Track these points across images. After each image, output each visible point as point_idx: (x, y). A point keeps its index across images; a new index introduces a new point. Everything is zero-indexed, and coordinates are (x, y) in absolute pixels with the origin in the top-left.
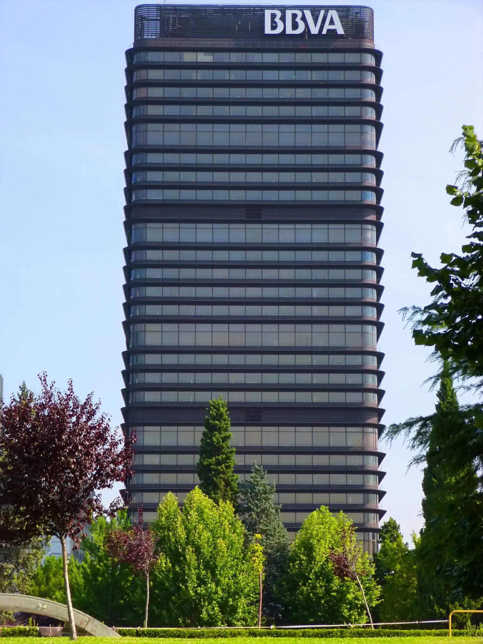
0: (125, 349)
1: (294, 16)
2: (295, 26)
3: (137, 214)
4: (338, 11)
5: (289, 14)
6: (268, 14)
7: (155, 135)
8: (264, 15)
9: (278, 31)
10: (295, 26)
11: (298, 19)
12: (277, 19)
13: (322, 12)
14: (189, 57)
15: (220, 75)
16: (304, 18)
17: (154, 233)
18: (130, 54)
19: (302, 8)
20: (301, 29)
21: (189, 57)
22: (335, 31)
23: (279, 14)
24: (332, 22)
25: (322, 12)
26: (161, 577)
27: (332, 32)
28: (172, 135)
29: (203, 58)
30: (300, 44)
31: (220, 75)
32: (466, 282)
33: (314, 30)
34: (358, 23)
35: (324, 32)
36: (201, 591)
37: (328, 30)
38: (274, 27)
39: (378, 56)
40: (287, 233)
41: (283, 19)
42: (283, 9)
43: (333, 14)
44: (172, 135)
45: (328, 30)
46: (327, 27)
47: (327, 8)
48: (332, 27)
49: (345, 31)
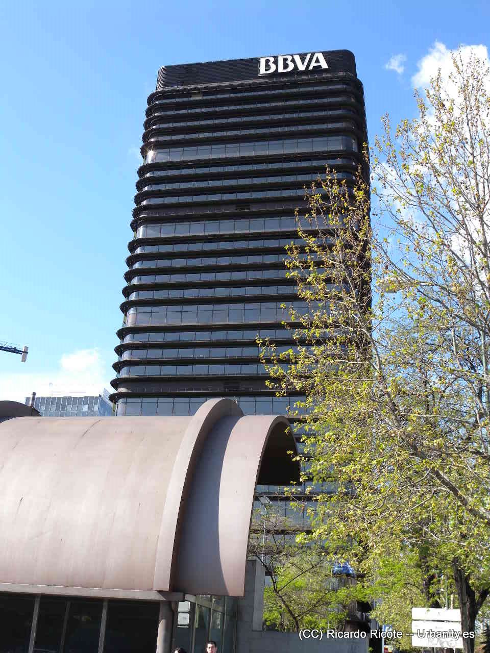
9: (273, 68)
11: (289, 62)
12: (271, 64)
16: (293, 61)
20: (291, 67)
24: (317, 61)
27: (318, 69)
34: (342, 61)
35: (311, 68)
38: (268, 67)
41: (276, 62)
45: (314, 67)
46: (313, 64)
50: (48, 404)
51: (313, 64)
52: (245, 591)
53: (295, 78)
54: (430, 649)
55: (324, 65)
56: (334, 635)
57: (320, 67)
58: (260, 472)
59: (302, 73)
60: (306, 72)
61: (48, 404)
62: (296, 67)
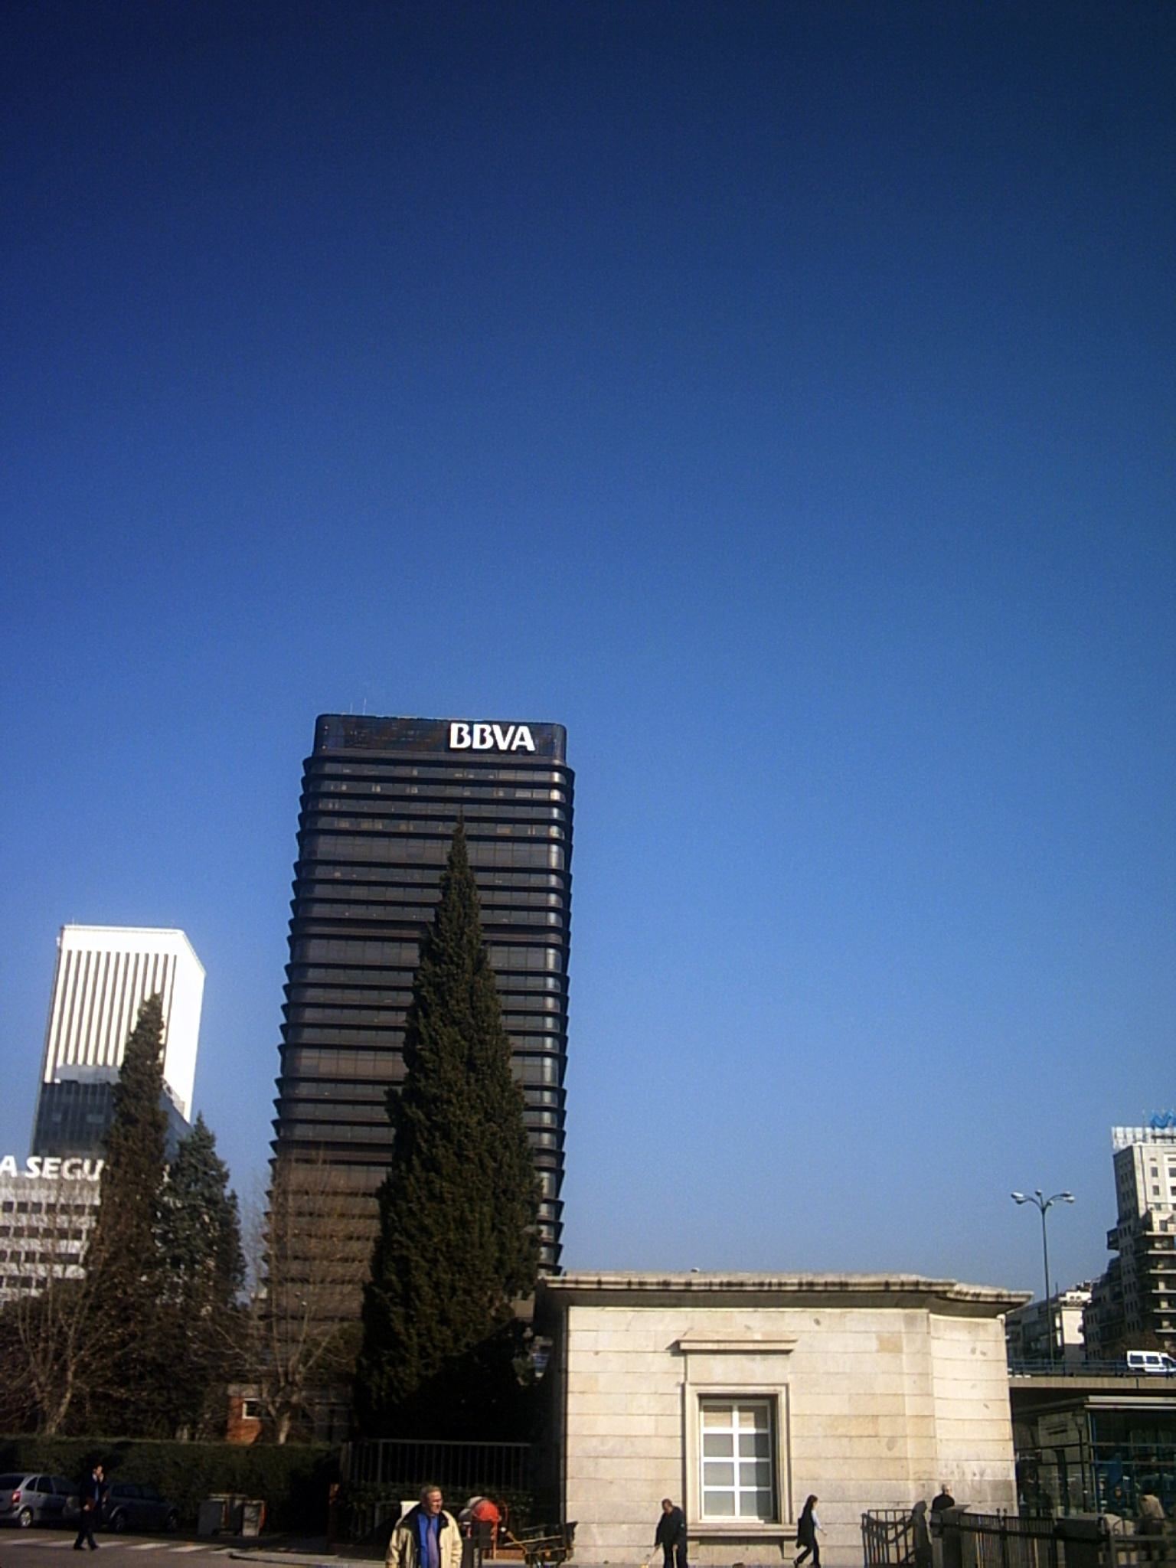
0: (279, 1075)
1: (483, 731)
2: (483, 741)
5: (477, 728)
6: (454, 727)
7: (326, 847)
8: (449, 730)
9: (465, 744)
10: (483, 741)
11: (487, 734)
16: (492, 734)
18: (307, 763)
20: (489, 744)
23: (466, 728)
24: (522, 739)
25: (512, 729)
27: (522, 749)
30: (488, 758)
32: (444, 1276)
35: (514, 748)
36: (41, 1166)
38: (461, 740)
39: (568, 774)
41: (471, 733)
43: (524, 730)
45: (519, 747)
46: (517, 742)
50: (94, 1093)
51: (517, 742)
52: (1026, 1469)
53: (497, 759)
54: (537, 1181)
55: (531, 747)
57: (525, 747)
58: (558, 1485)
59: (503, 752)
60: (509, 751)
61: (94, 1093)
62: (495, 743)
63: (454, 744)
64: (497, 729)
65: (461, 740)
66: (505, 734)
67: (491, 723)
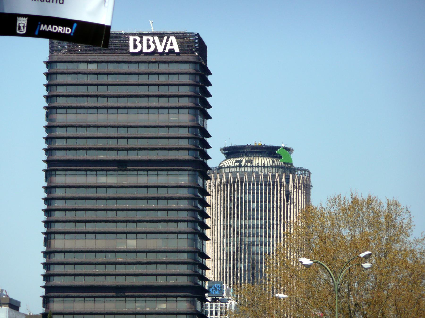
1: (148, 40)
2: (149, 47)
3: (53, 166)
4: (177, 37)
5: (145, 38)
6: (131, 38)
10: (149, 47)
11: (151, 42)
12: (137, 43)
13: (165, 38)
14: (82, 67)
15: (104, 79)
16: (154, 42)
17: (59, 179)
19: (153, 35)
21: (82, 67)
22: (173, 49)
24: (171, 44)
25: (165, 38)
26: (292, 264)
27: (172, 51)
28: (71, 118)
29: (93, 68)
31: (104, 79)
33: (160, 50)
35: (167, 51)
37: (170, 49)
38: (135, 47)
40: (142, 179)
41: (141, 42)
42: (141, 35)
43: (173, 39)
44: (71, 118)
46: (168, 47)
47: (169, 35)
48: (171, 47)
49: (180, 50)
51: (168, 47)
55: (177, 50)
56: (63, 30)
57: (173, 49)
63: (132, 49)
64: (156, 38)
65: (135, 47)
66: (161, 44)
67: (153, 35)
